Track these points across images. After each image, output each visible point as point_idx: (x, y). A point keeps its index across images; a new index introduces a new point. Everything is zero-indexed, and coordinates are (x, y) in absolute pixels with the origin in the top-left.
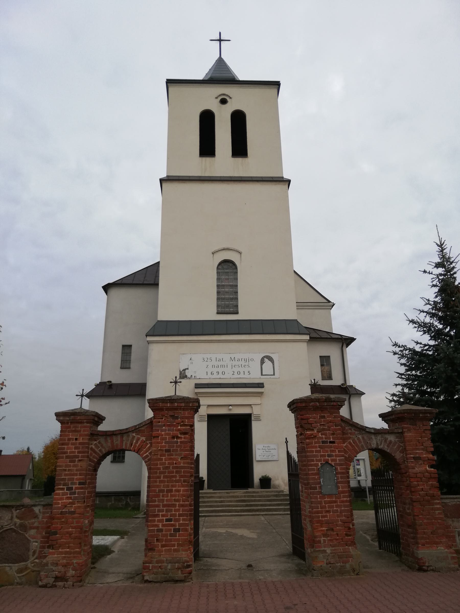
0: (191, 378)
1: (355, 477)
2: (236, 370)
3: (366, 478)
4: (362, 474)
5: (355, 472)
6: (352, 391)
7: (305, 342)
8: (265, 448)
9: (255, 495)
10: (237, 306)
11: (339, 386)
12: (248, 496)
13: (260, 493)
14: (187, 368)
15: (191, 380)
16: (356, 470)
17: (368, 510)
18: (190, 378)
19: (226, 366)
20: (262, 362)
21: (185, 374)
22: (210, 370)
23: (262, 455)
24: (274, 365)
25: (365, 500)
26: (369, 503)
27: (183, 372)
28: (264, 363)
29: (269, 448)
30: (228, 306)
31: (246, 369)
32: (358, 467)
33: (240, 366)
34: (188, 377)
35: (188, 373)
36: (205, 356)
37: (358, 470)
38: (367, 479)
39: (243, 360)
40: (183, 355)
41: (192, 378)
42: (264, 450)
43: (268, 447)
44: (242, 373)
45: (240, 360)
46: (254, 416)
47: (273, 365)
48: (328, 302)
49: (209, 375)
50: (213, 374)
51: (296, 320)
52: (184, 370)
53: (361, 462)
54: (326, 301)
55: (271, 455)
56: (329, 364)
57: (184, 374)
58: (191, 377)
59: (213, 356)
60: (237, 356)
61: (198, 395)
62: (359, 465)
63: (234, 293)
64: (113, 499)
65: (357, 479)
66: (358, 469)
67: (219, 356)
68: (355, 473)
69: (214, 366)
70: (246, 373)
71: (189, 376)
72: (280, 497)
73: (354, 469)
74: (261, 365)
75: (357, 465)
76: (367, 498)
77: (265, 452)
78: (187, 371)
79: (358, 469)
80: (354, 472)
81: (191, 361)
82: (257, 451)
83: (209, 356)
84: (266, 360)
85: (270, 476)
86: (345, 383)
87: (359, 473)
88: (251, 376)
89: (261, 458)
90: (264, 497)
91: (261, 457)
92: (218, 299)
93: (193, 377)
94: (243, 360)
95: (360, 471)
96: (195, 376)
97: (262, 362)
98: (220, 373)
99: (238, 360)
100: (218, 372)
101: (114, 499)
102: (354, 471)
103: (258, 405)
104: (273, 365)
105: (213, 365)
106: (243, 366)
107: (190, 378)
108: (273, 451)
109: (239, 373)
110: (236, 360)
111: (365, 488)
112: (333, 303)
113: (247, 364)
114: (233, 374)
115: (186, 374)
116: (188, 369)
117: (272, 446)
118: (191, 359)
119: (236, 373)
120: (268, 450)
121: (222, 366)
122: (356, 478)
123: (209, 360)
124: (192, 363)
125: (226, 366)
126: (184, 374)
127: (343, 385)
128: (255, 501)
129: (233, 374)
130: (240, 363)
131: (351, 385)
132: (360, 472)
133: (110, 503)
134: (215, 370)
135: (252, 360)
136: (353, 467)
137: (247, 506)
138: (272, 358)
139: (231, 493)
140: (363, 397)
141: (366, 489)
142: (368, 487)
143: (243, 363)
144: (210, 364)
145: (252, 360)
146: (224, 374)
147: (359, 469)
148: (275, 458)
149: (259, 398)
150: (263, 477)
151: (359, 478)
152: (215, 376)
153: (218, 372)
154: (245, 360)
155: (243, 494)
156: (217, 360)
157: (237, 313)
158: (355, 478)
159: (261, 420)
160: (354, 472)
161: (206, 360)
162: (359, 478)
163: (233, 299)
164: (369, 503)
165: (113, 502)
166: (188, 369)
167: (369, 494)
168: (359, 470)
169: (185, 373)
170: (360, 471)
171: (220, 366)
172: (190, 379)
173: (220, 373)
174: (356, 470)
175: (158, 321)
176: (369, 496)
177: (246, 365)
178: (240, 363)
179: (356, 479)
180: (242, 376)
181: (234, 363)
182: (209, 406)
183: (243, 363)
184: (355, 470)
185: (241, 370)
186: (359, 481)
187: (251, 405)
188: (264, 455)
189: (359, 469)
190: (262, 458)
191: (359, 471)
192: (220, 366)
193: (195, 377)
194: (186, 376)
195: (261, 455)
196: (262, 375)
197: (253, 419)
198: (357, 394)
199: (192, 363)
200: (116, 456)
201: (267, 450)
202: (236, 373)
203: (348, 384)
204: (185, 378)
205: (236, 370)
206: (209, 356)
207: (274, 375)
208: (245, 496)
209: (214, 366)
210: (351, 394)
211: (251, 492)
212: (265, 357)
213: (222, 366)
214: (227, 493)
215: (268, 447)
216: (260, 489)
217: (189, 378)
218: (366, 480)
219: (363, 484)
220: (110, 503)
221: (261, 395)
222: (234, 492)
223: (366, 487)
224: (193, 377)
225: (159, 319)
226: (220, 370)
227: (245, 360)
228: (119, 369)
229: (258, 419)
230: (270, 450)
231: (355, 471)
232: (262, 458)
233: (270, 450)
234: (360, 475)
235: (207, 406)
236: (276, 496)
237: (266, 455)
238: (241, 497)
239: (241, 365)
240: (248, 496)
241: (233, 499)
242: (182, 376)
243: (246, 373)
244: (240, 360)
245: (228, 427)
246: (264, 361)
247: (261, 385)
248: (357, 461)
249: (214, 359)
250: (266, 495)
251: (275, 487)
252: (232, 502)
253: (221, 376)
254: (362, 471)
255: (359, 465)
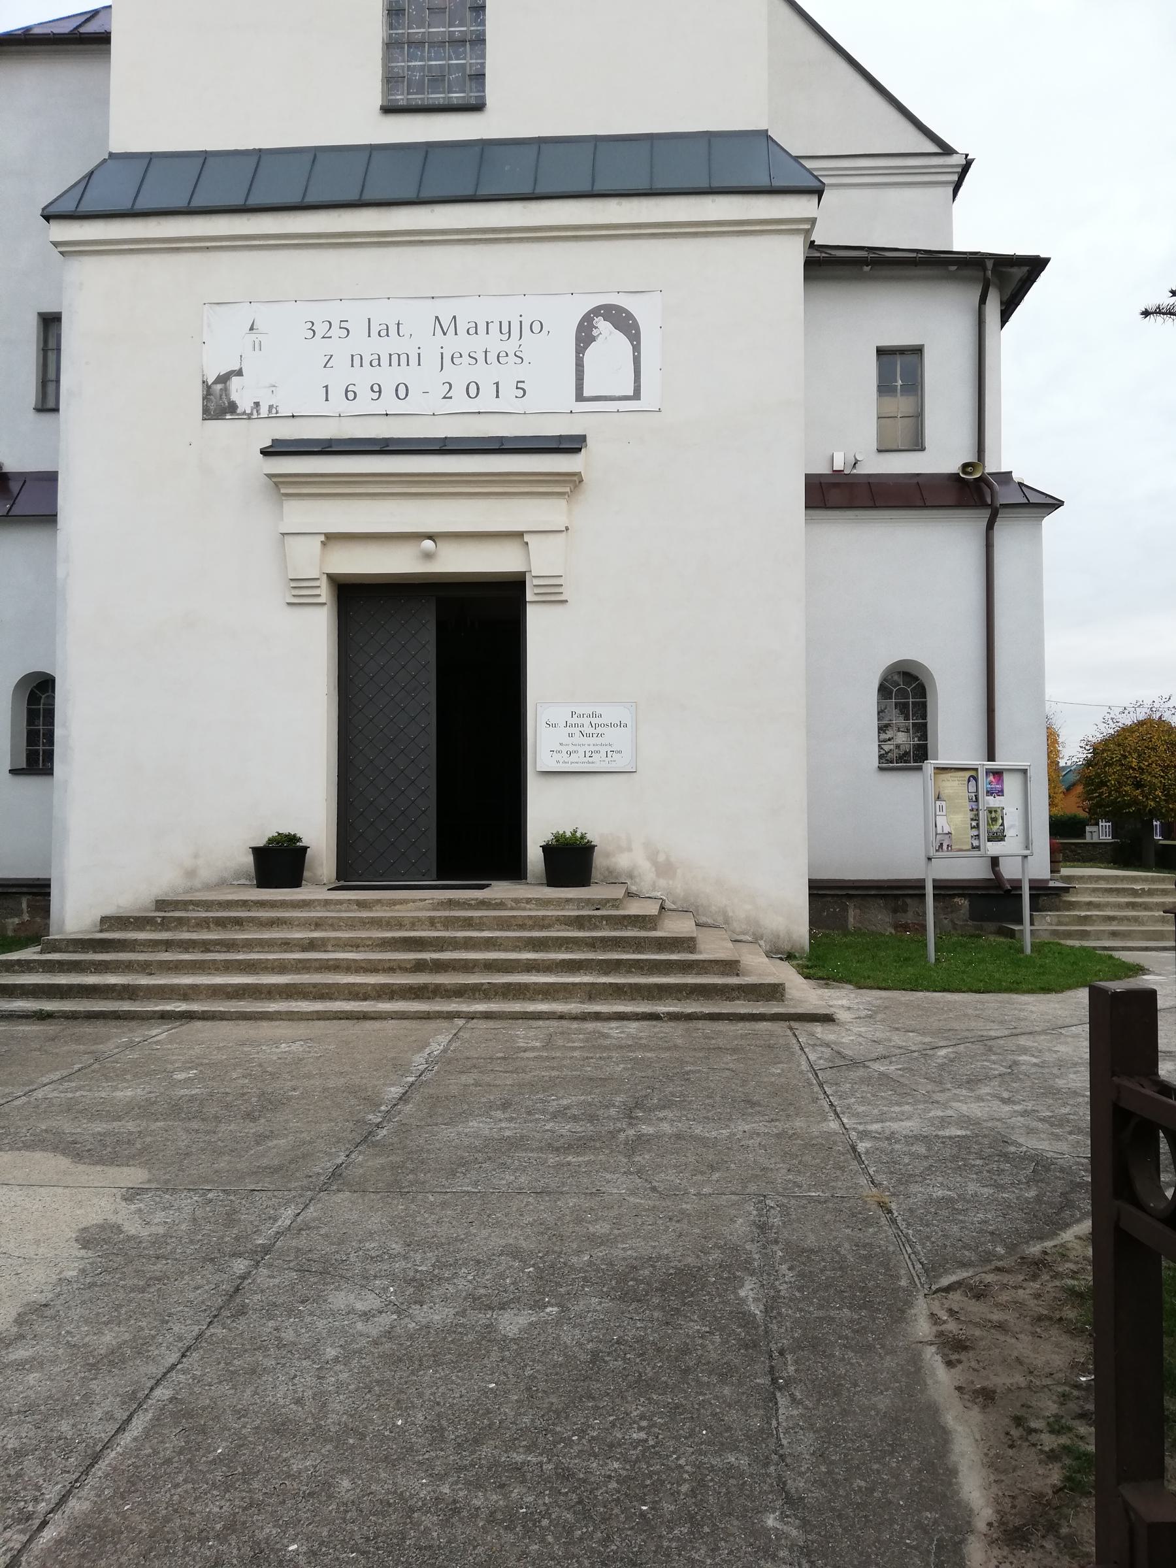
0: (255, 416)
1: (976, 843)
2: (460, 375)
3: (1027, 848)
4: (937, 853)
5: (978, 824)
6: (1005, 496)
7: (797, 231)
8: (580, 721)
9: (481, 917)
10: (479, 77)
11: (955, 477)
12: (448, 923)
13: (512, 909)
14: (237, 368)
15: (254, 424)
16: (983, 816)
17: (1014, 988)
18: (249, 417)
19: (413, 360)
20: (585, 336)
21: (228, 396)
22: (338, 379)
23: (564, 749)
24: (639, 353)
25: (1011, 934)
26: (1028, 951)
27: (219, 387)
28: (593, 339)
29: (594, 721)
30: (437, 80)
31: (508, 374)
32: (993, 802)
33: (480, 356)
34: (239, 411)
35: (241, 393)
36: (319, 312)
37: (993, 815)
38: (1027, 852)
39: (494, 328)
40: (217, 308)
41: (258, 414)
42: (576, 730)
43: (594, 715)
44: (488, 390)
45: (482, 328)
46: (536, 582)
47: (636, 348)
48: (939, 151)
49: (338, 403)
50: (355, 393)
51: (764, 134)
52: (224, 379)
53: (1011, 784)
54: (932, 148)
55: (603, 750)
56: (914, 386)
57: (221, 396)
58: (255, 412)
59: (356, 315)
60: (468, 311)
61: (283, 491)
62: (1001, 793)
63: (468, 13)
64: (24, 905)
65: (986, 850)
66: (990, 811)
67: (383, 313)
68: (978, 826)
69: (357, 360)
70: (508, 390)
71: (244, 405)
72: (595, 928)
73: (972, 810)
74: (578, 353)
75: (989, 793)
76: (1020, 921)
77: (578, 739)
78: (235, 381)
79: (990, 812)
80: (974, 823)
81: (253, 337)
82: (543, 731)
83: (335, 312)
84: (603, 326)
85: (593, 837)
86: (979, 459)
87: (995, 828)
88: (530, 404)
89: (558, 762)
90: (522, 927)
91: (557, 756)
92: (391, 45)
93: (264, 411)
94: (494, 328)
95: (1000, 821)
96: (271, 407)
97: (585, 336)
98: (388, 391)
99: (472, 331)
100: (376, 388)
101: (28, 906)
102: (972, 820)
103: (551, 537)
104: (636, 348)
105: (352, 356)
106: (492, 357)
107: (252, 414)
108: (611, 734)
109: (473, 390)
110: (462, 329)
111: (1017, 885)
112: (967, 155)
113: (511, 346)
114: (444, 398)
115: (234, 397)
116: (239, 373)
117: (610, 714)
118: (252, 329)
119: (459, 391)
120: (592, 730)
121: (395, 358)
122: (978, 848)
123: (336, 332)
124: (257, 346)
125: (413, 360)
126: (224, 397)
127: (969, 469)
128: (469, 944)
129: (444, 398)
130: (477, 344)
131: (1003, 470)
132: (1002, 825)
133: (17, 921)
134: (363, 378)
135: (537, 327)
136: (970, 800)
137: (420, 967)
138: (630, 316)
139: (378, 907)
140: (1051, 521)
141: (1020, 888)
142: (1030, 881)
143: (494, 342)
144: (342, 349)
145: (537, 327)
146: (407, 395)
147: (996, 811)
148: (620, 763)
149: (562, 503)
150: (557, 837)
151: (993, 848)
152: (365, 403)
153: (376, 388)
154: (505, 329)
155: (434, 910)
156: (374, 333)
157: (478, 107)
158: (973, 848)
159: (566, 601)
160: (974, 823)
161: (321, 329)
162: (993, 848)
163: (463, 42)
164: (1028, 951)
165: (26, 917)
166: (239, 373)
167: (1031, 910)
168: (994, 815)
169: (226, 390)
170: (1000, 821)
171: (385, 361)
172: (249, 419)
173: (388, 391)
174: (983, 816)
175: (111, 155)
176: (1031, 915)
177: (507, 355)
178: (477, 344)
179: (976, 853)
180: (486, 401)
181: (452, 344)
182: (331, 538)
183: (494, 342)
184: (978, 815)
185: (486, 375)
186: (995, 861)
187: (520, 535)
188: (571, 748)
189: (999, 810)
190: (564, 762)
191: (994, 820)
192: (385, 361)
193: (274, 411)
194: (232, 408)
195: (560, 748)
196: (580, 397)
197: (529, 596)
198: (1029, 505)
199: (257, 346)
200: (43, 750)
201: (587, 729)
202: (459, 391)
203: (991, 467)
204: (225, 413)
205: (460, 375)
206: (335, 312)
207: (637, 395)
208: (432, 923)
209: (357, 360)
210: (1002, 505)
211: (473, 902)
212: (596, 311)
213: (395, 358)
214: (361, 904)
215: (594, 715)
216: (542, 884)
217: (244, 413)
218: (1026, 857)
219: (1010, 871)
220: (17, 921)
221: (568, 490)
222: (393, 903)
223: (1020, 881)
224: (261, 411)
225: (116, 149)
226: (388, 377)
227: (505, 329)
228: (32, 414)
229: (554, 597)
230: (599, 730)
231: (976, 818)
232: (564, 762)
233: (599, 730)
234: (998, 837)
235: (322, 538)
236: (579, 922)
237: (581, 750)
238: (414, 924)
239: (486, 352)
240: (448, 923)
241: (363, 934)
242: (212, 406)
243: (508, 390)
244: (482, 328)
245: (429, 637)
246: (595, 332)
247: (571, 445)
248: (991, 778)
249: (358, 328)
250: (530, 917)
251: (613, 879)
252: (358, 946)
253: (388, 403)
254: (1012, 821)
255: (1001, 793)
